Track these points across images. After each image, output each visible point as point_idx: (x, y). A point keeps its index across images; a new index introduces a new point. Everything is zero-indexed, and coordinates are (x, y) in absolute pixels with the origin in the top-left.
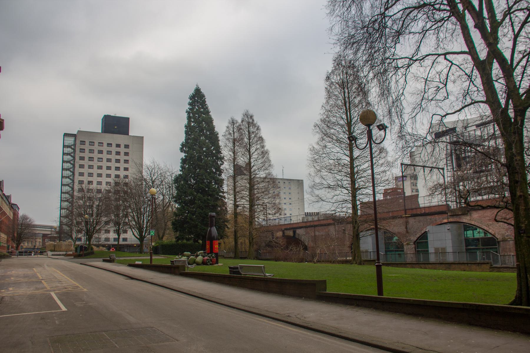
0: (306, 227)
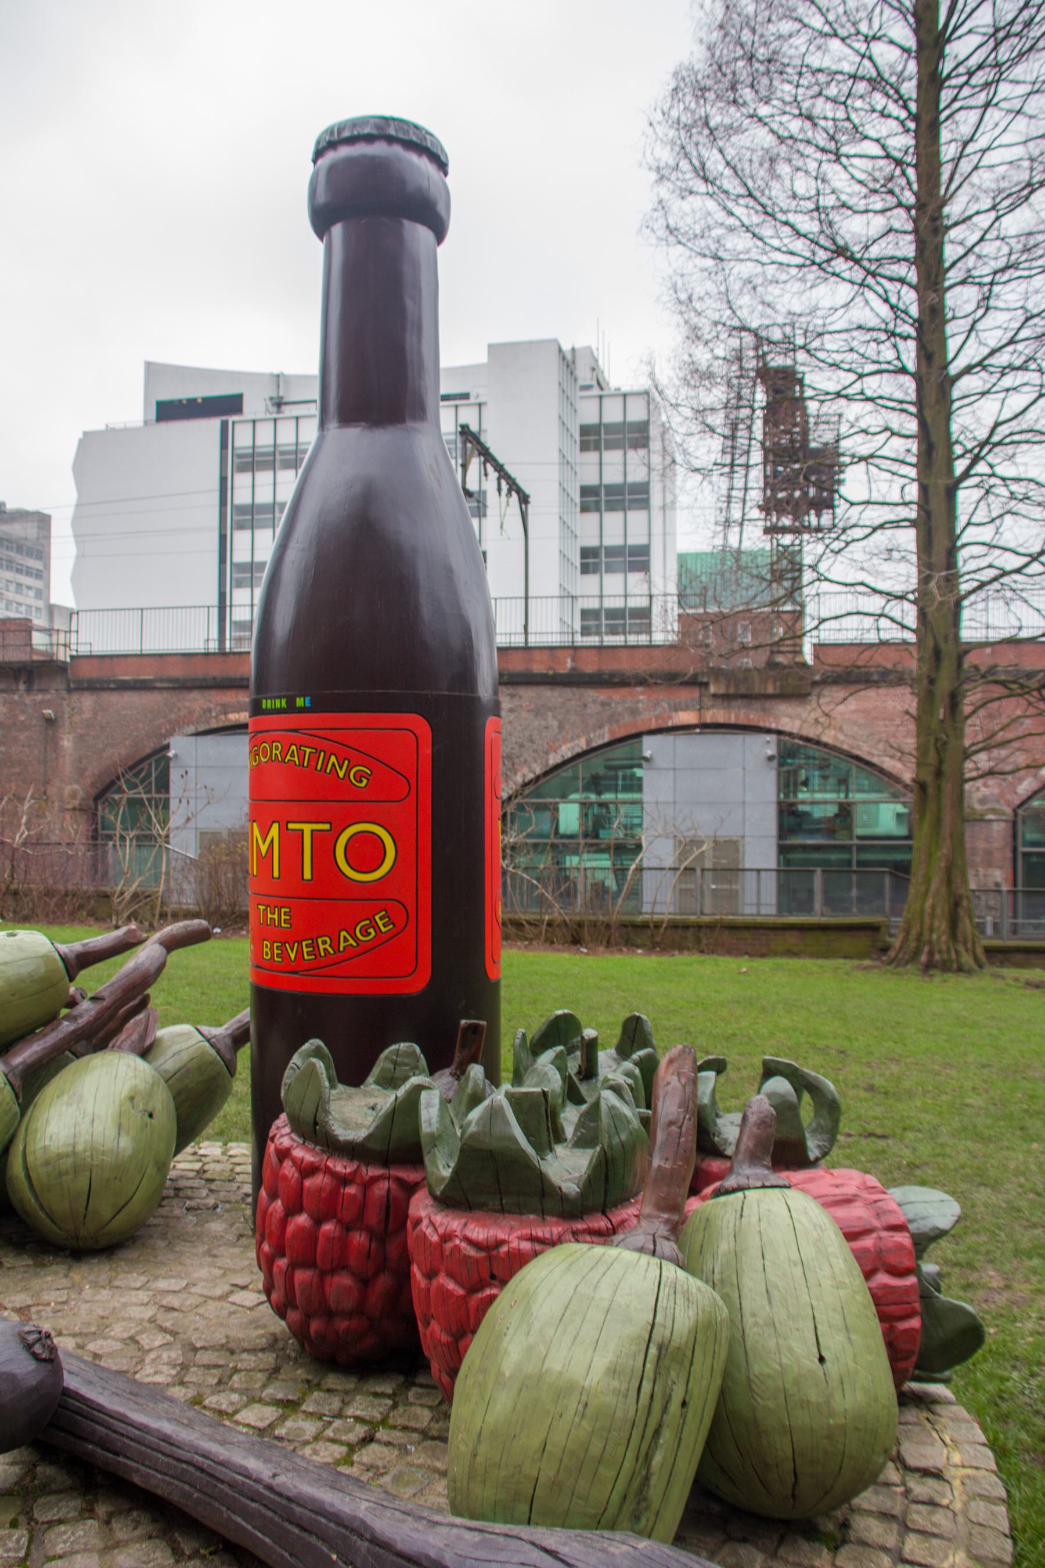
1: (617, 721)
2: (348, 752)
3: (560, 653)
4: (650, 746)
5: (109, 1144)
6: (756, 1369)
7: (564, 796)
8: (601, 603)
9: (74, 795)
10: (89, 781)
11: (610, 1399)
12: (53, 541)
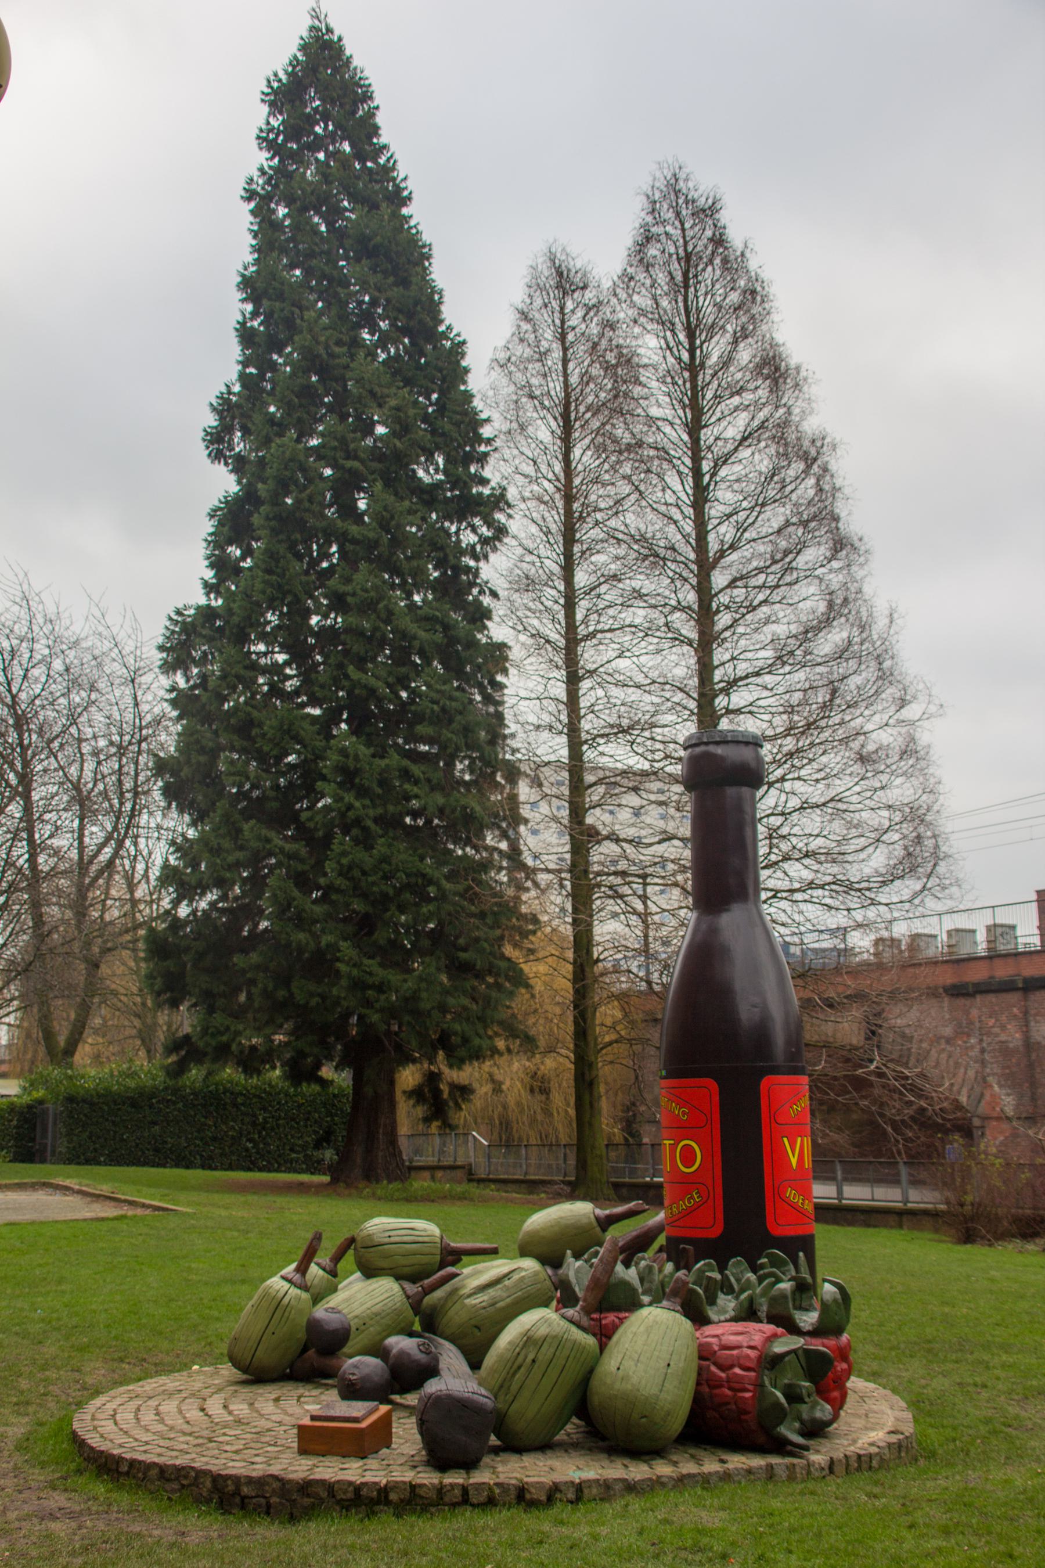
0: (959, 991)
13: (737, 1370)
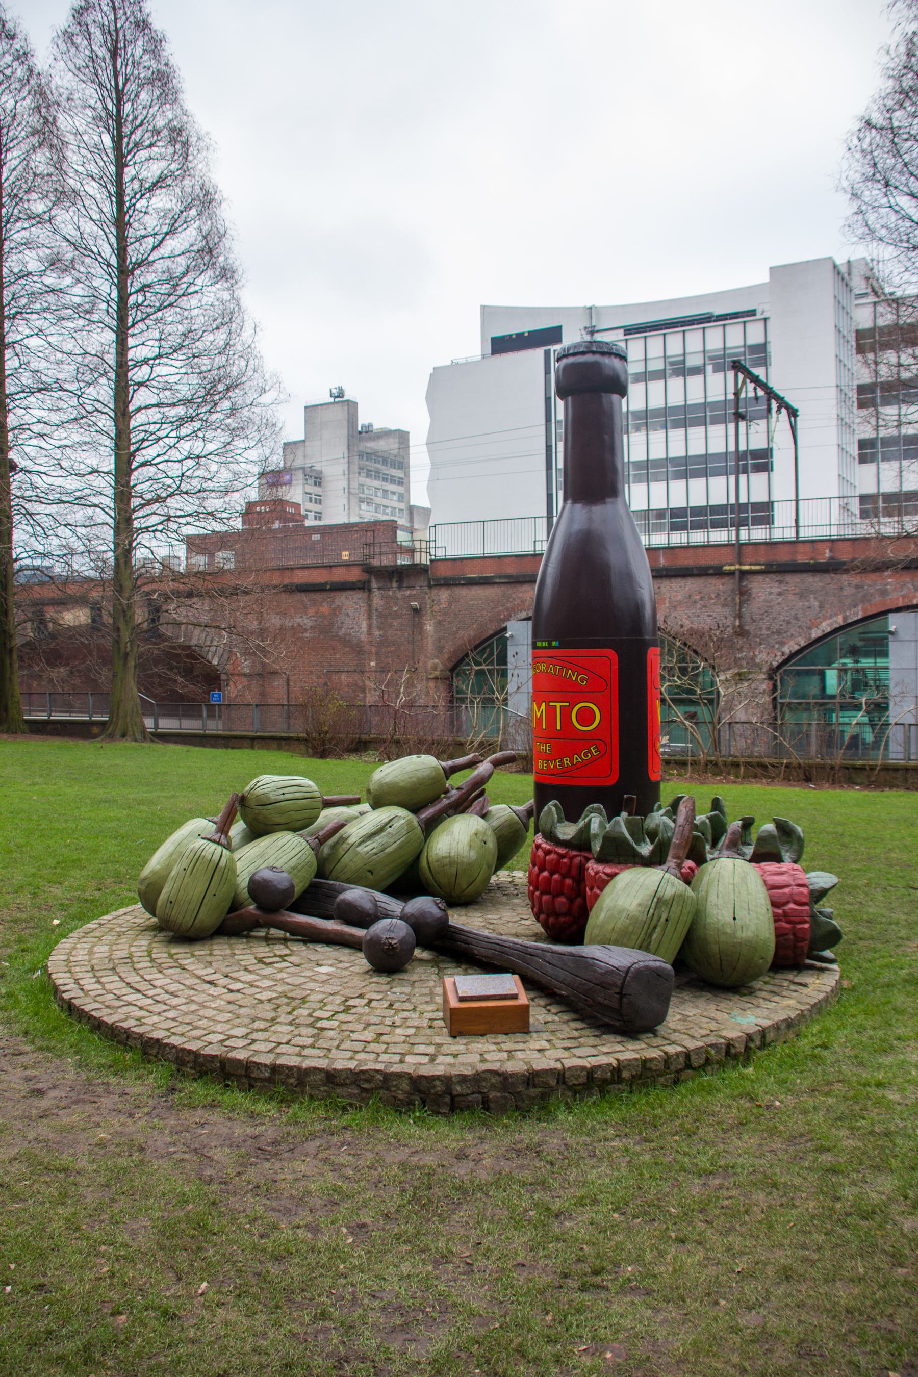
1: (869, 601)
2: (576, 667)
3: (820, 545)
4: (894, 622)
5: (466, 854)
6: (709, 920)
7: (829, 664)
8: (797, 532)
9: (435, 668)
10: (446, 656)
11: (637, 913)
12: (411, 450)
13: (792, 906)
